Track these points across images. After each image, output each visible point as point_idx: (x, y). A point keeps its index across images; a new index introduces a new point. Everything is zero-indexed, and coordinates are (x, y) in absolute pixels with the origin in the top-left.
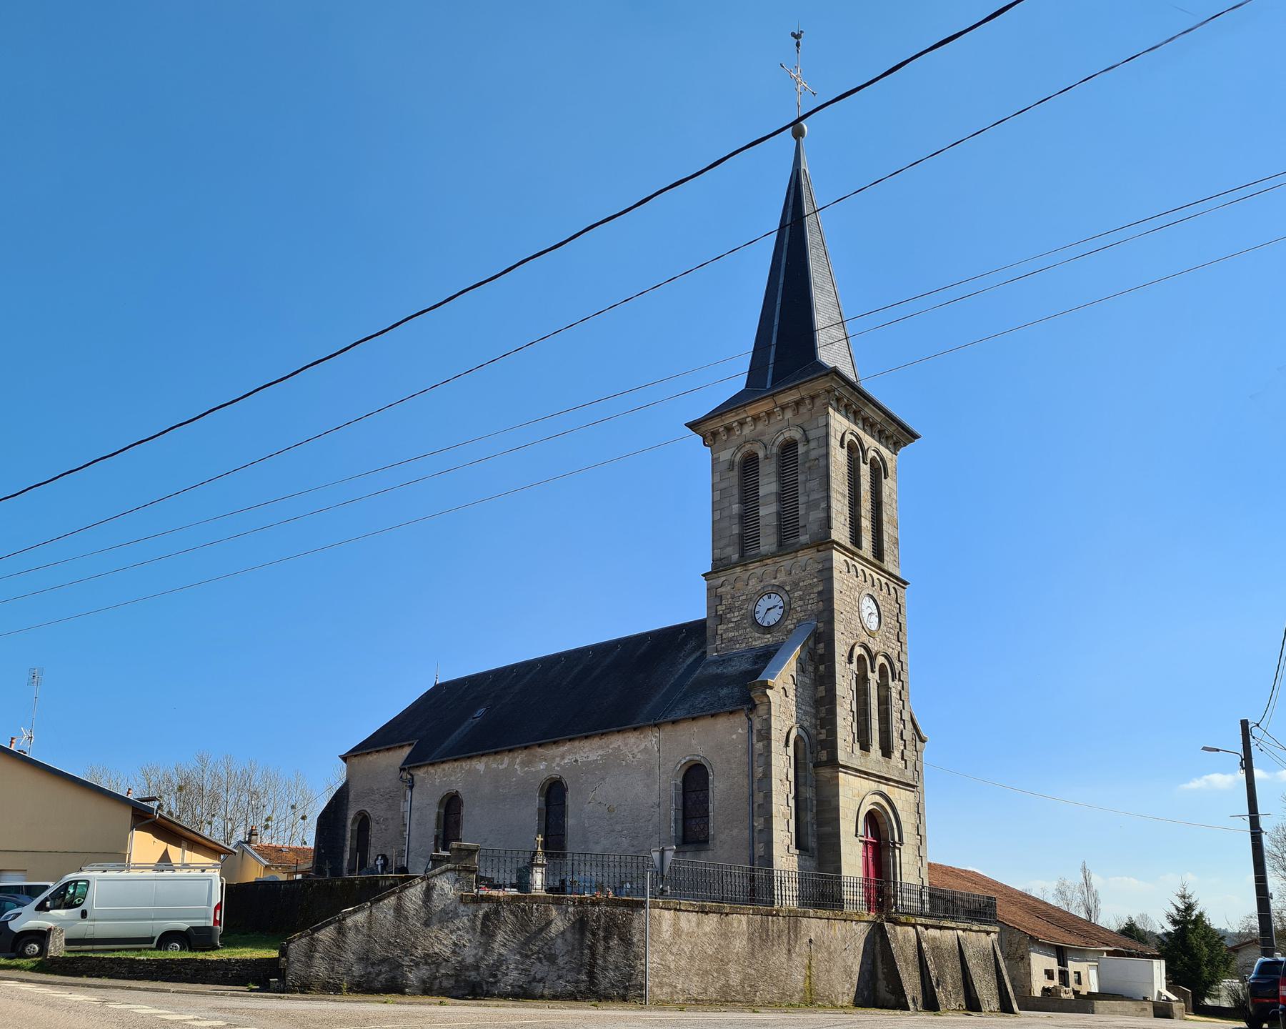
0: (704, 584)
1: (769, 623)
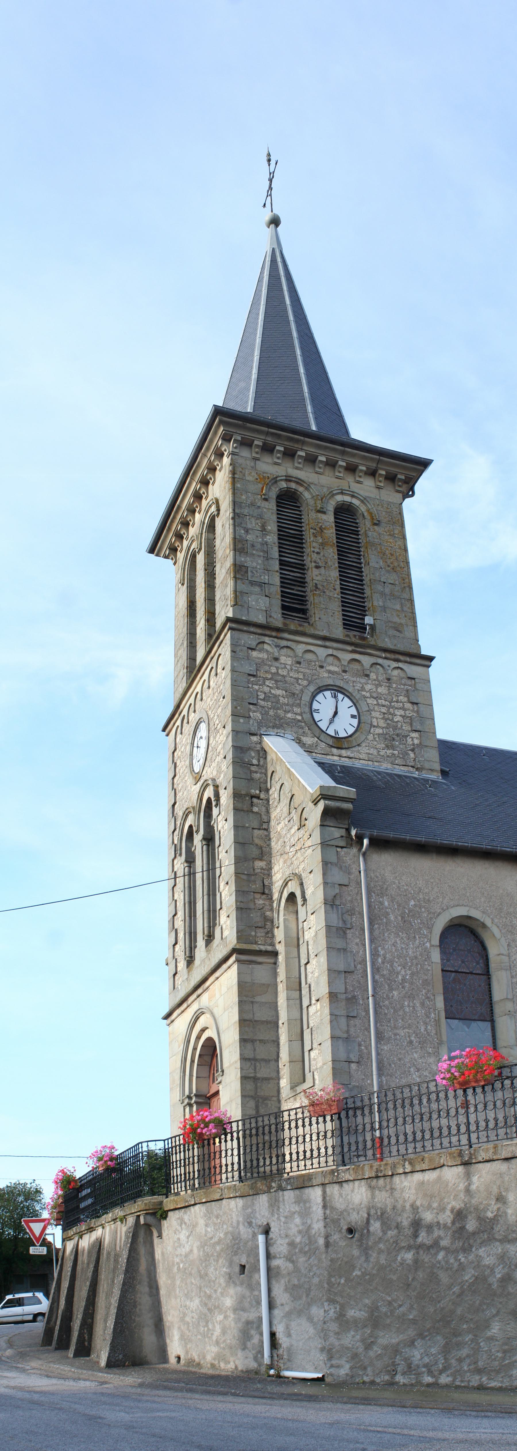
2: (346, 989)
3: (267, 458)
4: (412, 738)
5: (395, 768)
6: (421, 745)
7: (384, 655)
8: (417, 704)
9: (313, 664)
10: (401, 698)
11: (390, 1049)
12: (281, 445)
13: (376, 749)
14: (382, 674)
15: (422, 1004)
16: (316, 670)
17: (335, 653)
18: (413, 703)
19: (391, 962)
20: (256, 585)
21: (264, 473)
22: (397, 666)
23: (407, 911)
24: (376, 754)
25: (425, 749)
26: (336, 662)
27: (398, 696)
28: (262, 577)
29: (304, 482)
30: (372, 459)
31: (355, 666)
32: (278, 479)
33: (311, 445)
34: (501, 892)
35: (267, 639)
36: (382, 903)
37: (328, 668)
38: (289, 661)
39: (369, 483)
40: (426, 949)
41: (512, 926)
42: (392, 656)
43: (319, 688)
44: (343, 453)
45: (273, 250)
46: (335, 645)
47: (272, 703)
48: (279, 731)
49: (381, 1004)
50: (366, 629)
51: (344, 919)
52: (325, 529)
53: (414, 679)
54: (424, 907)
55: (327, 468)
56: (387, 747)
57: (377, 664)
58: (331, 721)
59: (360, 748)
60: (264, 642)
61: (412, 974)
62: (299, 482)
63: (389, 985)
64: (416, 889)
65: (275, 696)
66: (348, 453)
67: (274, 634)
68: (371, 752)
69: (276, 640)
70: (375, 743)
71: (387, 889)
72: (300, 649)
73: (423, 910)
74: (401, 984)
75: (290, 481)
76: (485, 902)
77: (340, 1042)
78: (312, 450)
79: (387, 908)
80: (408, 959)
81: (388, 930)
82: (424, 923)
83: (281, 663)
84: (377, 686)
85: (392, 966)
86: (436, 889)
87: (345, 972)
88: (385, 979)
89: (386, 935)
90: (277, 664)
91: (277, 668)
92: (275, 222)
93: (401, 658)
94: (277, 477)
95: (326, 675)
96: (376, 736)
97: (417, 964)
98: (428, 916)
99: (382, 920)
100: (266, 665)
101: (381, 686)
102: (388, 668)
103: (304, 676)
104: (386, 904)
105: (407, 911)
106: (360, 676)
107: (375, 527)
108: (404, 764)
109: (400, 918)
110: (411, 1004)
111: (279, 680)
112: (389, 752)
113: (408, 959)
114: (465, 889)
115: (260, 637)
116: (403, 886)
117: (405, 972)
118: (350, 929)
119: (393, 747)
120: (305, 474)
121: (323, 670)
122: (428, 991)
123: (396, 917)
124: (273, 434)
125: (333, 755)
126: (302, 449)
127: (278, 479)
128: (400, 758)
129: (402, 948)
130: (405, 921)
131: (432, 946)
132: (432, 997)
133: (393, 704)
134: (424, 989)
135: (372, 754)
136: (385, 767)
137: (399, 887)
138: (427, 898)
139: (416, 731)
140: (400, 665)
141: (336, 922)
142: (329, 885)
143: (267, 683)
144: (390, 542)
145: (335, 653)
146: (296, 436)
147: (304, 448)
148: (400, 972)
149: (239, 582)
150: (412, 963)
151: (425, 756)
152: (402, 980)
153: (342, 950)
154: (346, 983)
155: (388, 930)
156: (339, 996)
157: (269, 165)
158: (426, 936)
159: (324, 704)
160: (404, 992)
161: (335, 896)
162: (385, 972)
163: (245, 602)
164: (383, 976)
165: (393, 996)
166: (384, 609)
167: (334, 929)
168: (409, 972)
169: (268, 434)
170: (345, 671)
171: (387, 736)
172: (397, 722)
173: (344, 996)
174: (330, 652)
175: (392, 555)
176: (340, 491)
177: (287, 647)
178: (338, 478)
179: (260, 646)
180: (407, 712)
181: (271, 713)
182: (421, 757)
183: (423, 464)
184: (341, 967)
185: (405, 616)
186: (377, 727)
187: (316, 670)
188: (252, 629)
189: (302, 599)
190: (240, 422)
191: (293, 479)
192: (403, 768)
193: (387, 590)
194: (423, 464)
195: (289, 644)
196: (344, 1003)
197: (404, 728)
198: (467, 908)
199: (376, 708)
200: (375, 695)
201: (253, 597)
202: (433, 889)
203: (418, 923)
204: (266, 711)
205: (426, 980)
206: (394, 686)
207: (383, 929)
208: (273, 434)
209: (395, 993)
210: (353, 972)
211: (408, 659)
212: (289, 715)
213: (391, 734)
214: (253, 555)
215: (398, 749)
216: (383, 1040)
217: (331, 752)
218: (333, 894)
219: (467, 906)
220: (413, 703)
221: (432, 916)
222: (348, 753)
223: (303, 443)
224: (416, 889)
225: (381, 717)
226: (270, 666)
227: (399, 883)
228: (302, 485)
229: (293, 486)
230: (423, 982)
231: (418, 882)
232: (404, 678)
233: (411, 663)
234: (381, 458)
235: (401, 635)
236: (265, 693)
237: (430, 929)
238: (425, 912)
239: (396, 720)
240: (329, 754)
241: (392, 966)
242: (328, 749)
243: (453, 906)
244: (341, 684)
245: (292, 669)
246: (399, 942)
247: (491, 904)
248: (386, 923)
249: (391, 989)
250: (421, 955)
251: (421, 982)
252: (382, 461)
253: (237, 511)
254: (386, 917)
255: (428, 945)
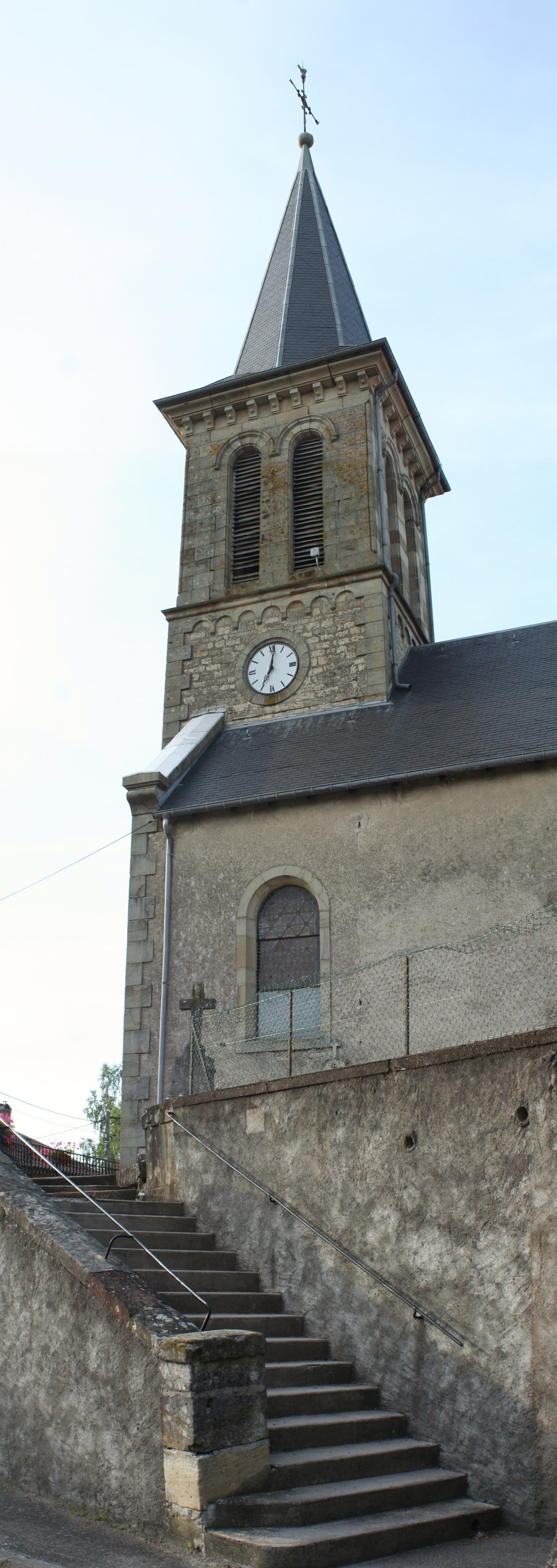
0: (163, 626)
1: (272, 688)
2: (143, 979)
3: (222, 423)
4: (357, 666)
5: (334, 706)
6: (366, 671)
7: (326, 585)
8: (364, 624)
9: (252, 623)
10: (347, 625)
11: (184, 1035)
12: (227, 405)
13: (314, 691)
14: (327, 606)
15: (223, 982)
16: (254, 629)
17: (274, 603)
18: (359, 625)
19: (192, 945)
20: (201, 563)
21: (218, 442)
22: (343, 590)
23: (214, 887)
24: (313, 697)
25: (369, 673)
26: (276, 612)
27: (343, 624)
28: (208, 553)
29: (256, 431)
30: (322, 371)
31: (296, 609)
32: (230, 441)
33: (254, 389)
34: (328, 838)
35: (204, 617)
36: (187, 884)
37: (267, 622)
38: (227, 630)
39: (331, 395)
40: (231, 922)
41: (338, 875)
42: (337, 582)
43: (256, 647)
44: (290, 380)
45: (306, 171)
46: (272, 595)
47: (207, 680)
48: (211, 708)
49: (178, 989)
50: (314, 561)
51: (147, 909)
52: (277, 471)
53: (362, 597)
54: (234, 878)
55: (305, 397)
56: (327, 685)
57: (320, 597)
58: (267, 678)
59: (295, 697)
60: (201, 621)
61: (215, 952)
62: (253, 433)
63: (188, 968)
64: (227, 860)
65: (210, 672)
66: (295, 378)
67: (209, 609)
68: (307, 698)
69: (212, 614)
70: (313, 685)
71: (195, 868)
72: (235, 614)
73: (233, 881)
74: (200, 965)
75: (244, 437)
76: (306, 855)
77: (132, 1034)
78: (259, 393)
79: (193, 888)
80: (211, 938)
81: (192, 911)
82: (232, 895)
83: (218, 636)
84: (320, 621)
85: (192, 948)
86: (249, 855)
87: (144, 963)
88: (184, 962)
89: (189, 917)
90: (214, 638)
91: (214, 643)
92: (307, 141)
93: (346, 579)
94: (229, 441)
95: (264, 630)
96: (314, 678)
97: (220, 941)
98: (237, 886)
99: (186, 902)
100: (203, 643)
101: (325, 619)
102: (332, 597)
103: (241, 640)
104: (193, 884)
105: (214, 887)
106: (302, 617)
107: (335, 444)
108: (345, 698)
109: (206, 896)
110: (210, 984)
111: (215, 655)
112: (328, 690)
113: (211, 938)
114: (283, 846)
115: (197, 617)
116: (213, 860)
117: (207, 951)
118: (152, 919)
119: (333, 684)
120: (246, 424)
121: (261, 626)
122: (230, 967)
123: (202, 896)
124: (216, 399)
125: (266, 714)
126: (250, 398)
127: (230, 441)
128: (341, 693)
129: (205, 927)
130: (211, 898)
131: (237, 918)
132: (234, 973)
133: (337, 635)
134: (226, 965)
135: (308, 700)
136: (324, 708)
137: (208, 863)
138: (238, 867)
139: (361, 656)
140: (347, 587)
141: (139, 914)
142: (136, 878)
143: (203, 662)
144: (351, 453)
145: (274, 603)
146: (238, 389)
147: (251, 396)
148: (201, 952)
149: (185, 567)
150: (215, 942)
151: (369, 682)
152: (203, 960)
153: (142, 943)
154: (143, 974)
155: (192, 911)
156: (135, 988)
157: (304, 82)
158: (232, 909)
159: (285, 657)
160: (203, 973)
161: (140, 889)
162: (185, 956)
163: (190, 586)
164: (183, 959)
165: (191, 979)
166: (336, 531)
167: (136, 923)
168: (211, 950)
169: (212, 401)
170: (284, 619)
171: (327, 674)
172: (339, 654)
173: (139, 988)
174: (268, 604)
175: (349, 466)
176: (296, 422)
177: (225, 616)
178: (296, 408)
179: (198, 626)
180: (353, 638)
181: (205, 692)
182: (364, 684)
183: (162, 404)
184: (140, 959)
185: (360, 529)
186: (318, 666)
187: (254, 629)
188: (188, 613)
189: (255, 557)
190: (182, 404)
191: (247, 434)
192: (343, 704)
193: (341, 509)
194: (162, 404)
195: (226, 613)
196: (139, 995)
197: (348, 657)
198: (284, 867)
199: (318, 646)
200: (317, 632)
201: (198, 577)
202: (246, 855)
203: (225, 896)
204: (199, 692)
205: (229, 955)
206: (340, 613)
207: (188, 912)
208: (216, 399)
209: (194, 975)
210: (151, 962)
211: (355, 578)
212: (223, 688)
213: (332, 669)
214: (201, 533)
215: (339, 684)
216: (176, 1026)
217: (264, 711)
218: (139, 886)
219: (285, 864)
220: (359, 625)
221: (242, 885)
222: (283, 707)
223: (248, 391)
224: (227, 860)
225: (321, 654)
226: (207, 643)
227: (209, 858)
228: (255, 436)
229: (248, 440)
230: (225, 958)
231: (230, 852)
232: (352, 600)
233: (358, 581)
234: (330, 365)
235: (355, 552)
236: (200, 673)
237: (238, 900)
238: (234, 883)
239: (338, 652)
240: (262, 715)
241: (192, 948)
242: (261, 709)
243: (269, 869)
244: (279, 634)
245: (229, 638)
246: (202, 922)
247: (313, 855)
248: (191, 904)
249: (190, 971)
250: (225, 930)
251: (223, 958)
252: (333, 367)
253: (188, 495)
254: (191, 898)
255: (234, 918)
